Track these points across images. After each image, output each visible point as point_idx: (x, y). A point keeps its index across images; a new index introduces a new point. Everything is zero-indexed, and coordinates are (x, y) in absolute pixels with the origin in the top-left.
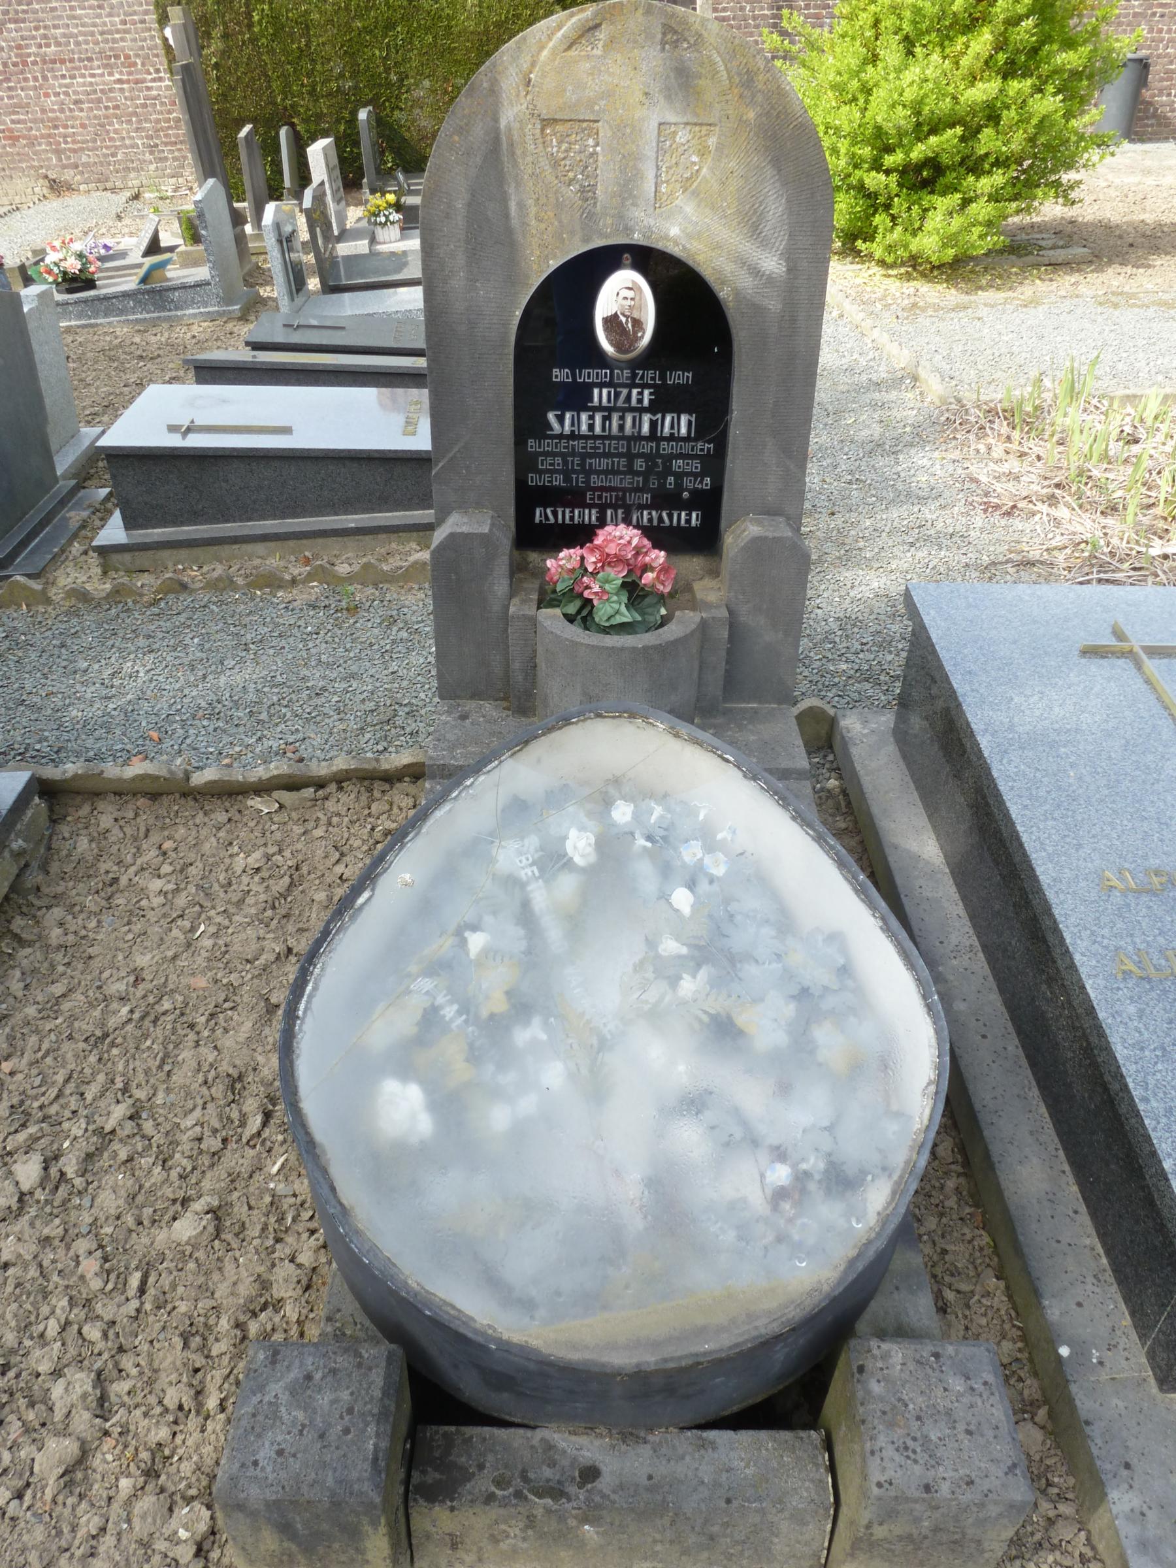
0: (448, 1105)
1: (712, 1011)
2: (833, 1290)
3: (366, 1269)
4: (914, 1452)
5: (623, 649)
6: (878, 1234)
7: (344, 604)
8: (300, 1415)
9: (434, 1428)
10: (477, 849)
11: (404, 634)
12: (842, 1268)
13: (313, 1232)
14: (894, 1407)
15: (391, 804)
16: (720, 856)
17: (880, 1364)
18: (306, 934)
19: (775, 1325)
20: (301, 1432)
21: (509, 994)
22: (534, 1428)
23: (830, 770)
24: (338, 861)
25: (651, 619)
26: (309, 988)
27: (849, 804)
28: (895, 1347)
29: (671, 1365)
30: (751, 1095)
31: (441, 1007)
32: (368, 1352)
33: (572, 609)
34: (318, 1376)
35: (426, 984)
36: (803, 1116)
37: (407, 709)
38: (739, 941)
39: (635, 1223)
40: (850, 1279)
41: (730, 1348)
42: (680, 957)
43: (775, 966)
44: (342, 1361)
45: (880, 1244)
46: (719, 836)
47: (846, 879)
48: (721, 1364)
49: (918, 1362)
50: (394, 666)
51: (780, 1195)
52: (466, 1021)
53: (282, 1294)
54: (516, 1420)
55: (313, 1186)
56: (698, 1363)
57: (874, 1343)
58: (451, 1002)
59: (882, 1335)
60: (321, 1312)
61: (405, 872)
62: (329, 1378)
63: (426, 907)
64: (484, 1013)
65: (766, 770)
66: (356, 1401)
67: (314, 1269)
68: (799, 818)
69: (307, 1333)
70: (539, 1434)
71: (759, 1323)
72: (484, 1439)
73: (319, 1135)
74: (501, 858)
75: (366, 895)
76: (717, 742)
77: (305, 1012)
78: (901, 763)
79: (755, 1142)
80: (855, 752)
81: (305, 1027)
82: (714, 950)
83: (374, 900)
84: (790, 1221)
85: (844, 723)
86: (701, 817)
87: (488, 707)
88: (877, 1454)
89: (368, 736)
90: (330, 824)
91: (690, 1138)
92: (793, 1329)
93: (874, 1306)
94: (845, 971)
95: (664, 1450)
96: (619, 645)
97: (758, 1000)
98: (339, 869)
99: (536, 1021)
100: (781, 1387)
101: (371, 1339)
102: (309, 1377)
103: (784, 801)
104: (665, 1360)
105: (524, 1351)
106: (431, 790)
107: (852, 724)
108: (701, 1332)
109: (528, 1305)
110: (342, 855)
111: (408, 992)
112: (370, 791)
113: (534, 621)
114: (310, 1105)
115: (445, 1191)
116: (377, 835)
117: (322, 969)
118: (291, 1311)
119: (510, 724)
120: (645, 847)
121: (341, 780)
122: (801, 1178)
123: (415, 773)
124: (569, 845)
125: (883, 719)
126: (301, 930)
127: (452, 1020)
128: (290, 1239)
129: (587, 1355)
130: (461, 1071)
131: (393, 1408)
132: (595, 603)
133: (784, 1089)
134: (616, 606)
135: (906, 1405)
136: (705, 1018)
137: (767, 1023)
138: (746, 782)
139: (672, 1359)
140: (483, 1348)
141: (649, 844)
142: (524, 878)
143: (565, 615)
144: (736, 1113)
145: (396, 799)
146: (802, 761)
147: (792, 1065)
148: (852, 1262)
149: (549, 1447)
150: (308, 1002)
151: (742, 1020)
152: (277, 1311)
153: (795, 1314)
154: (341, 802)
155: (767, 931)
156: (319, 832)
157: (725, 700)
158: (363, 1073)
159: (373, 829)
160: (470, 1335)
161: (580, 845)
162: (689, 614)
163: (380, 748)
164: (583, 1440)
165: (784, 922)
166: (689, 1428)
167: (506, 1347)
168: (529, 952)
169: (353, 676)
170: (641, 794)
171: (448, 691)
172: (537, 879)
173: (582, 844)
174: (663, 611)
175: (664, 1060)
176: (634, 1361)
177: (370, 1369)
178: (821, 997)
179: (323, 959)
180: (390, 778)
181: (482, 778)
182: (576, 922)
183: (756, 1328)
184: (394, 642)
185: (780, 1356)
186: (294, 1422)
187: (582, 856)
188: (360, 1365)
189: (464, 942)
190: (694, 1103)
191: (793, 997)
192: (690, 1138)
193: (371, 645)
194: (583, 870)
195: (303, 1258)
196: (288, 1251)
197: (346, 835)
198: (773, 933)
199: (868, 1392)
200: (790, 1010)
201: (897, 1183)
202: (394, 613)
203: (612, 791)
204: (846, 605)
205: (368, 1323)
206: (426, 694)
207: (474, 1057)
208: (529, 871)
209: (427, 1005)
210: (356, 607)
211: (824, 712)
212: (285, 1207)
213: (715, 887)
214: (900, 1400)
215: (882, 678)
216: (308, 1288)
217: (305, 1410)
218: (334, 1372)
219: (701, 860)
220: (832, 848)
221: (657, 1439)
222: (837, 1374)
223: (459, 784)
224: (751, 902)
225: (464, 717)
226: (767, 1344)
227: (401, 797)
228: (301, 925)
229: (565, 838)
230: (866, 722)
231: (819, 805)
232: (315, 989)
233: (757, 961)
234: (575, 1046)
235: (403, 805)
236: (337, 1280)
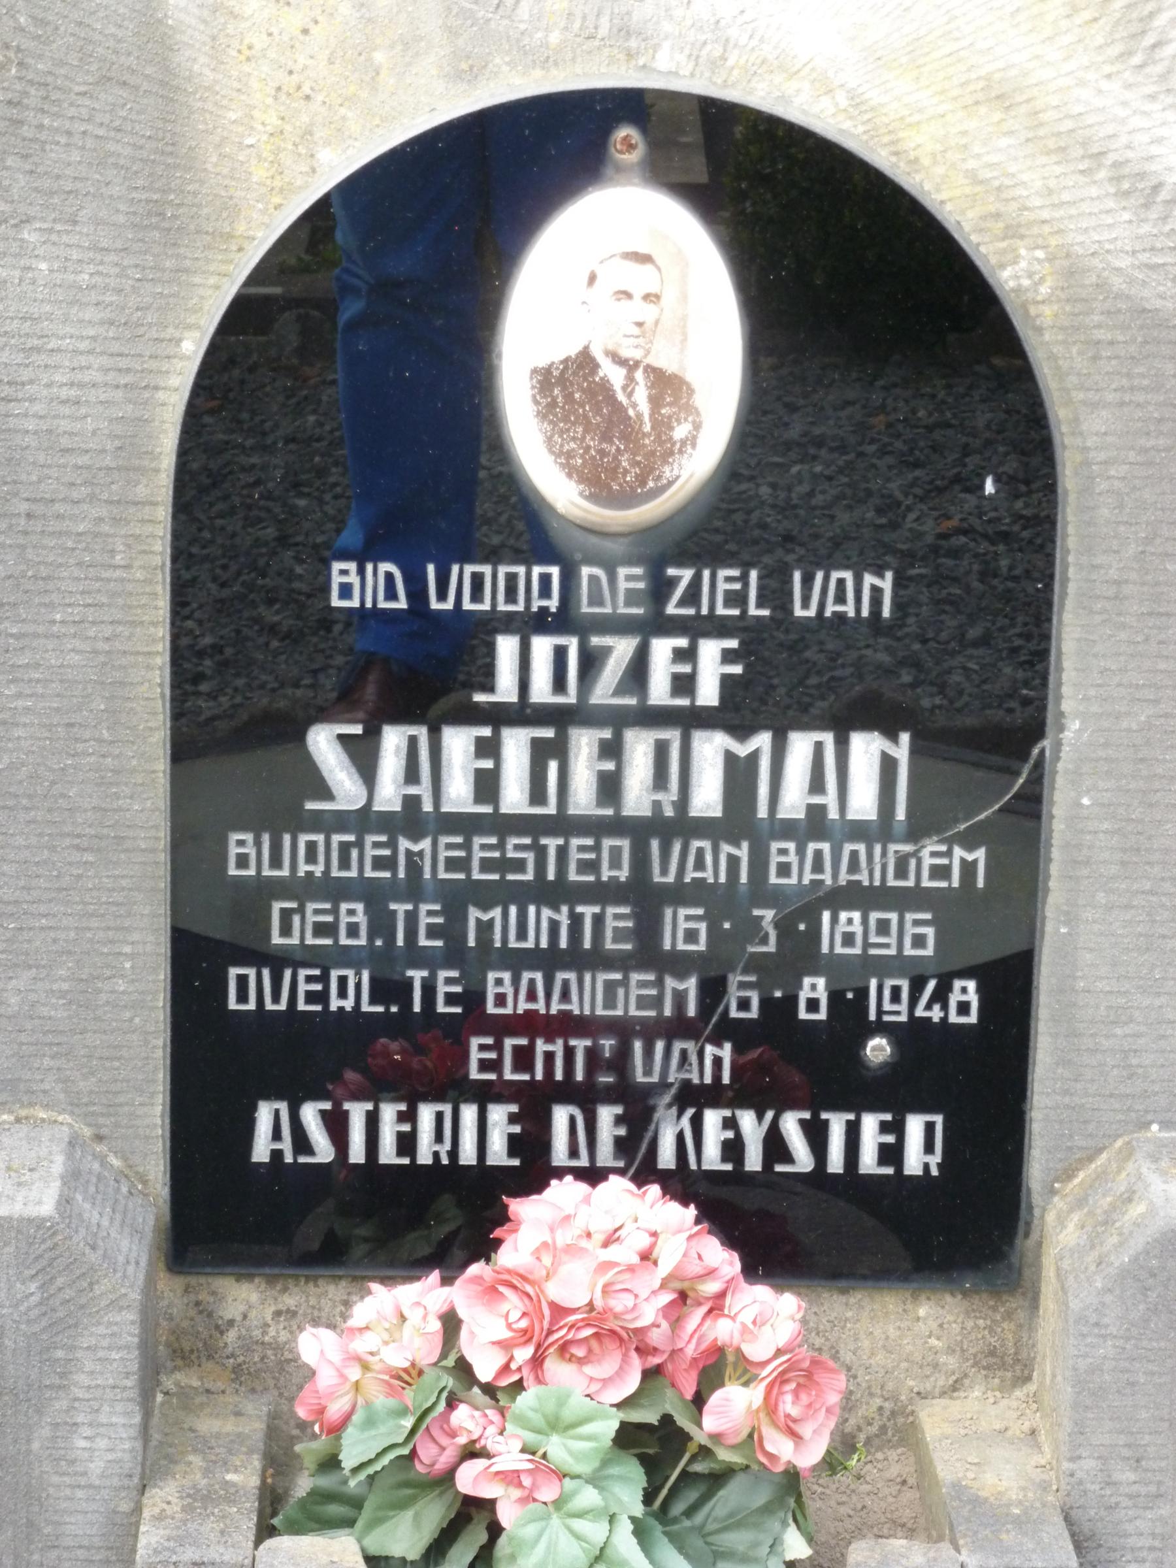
132: (506, 1514)
134: (596, 1531)
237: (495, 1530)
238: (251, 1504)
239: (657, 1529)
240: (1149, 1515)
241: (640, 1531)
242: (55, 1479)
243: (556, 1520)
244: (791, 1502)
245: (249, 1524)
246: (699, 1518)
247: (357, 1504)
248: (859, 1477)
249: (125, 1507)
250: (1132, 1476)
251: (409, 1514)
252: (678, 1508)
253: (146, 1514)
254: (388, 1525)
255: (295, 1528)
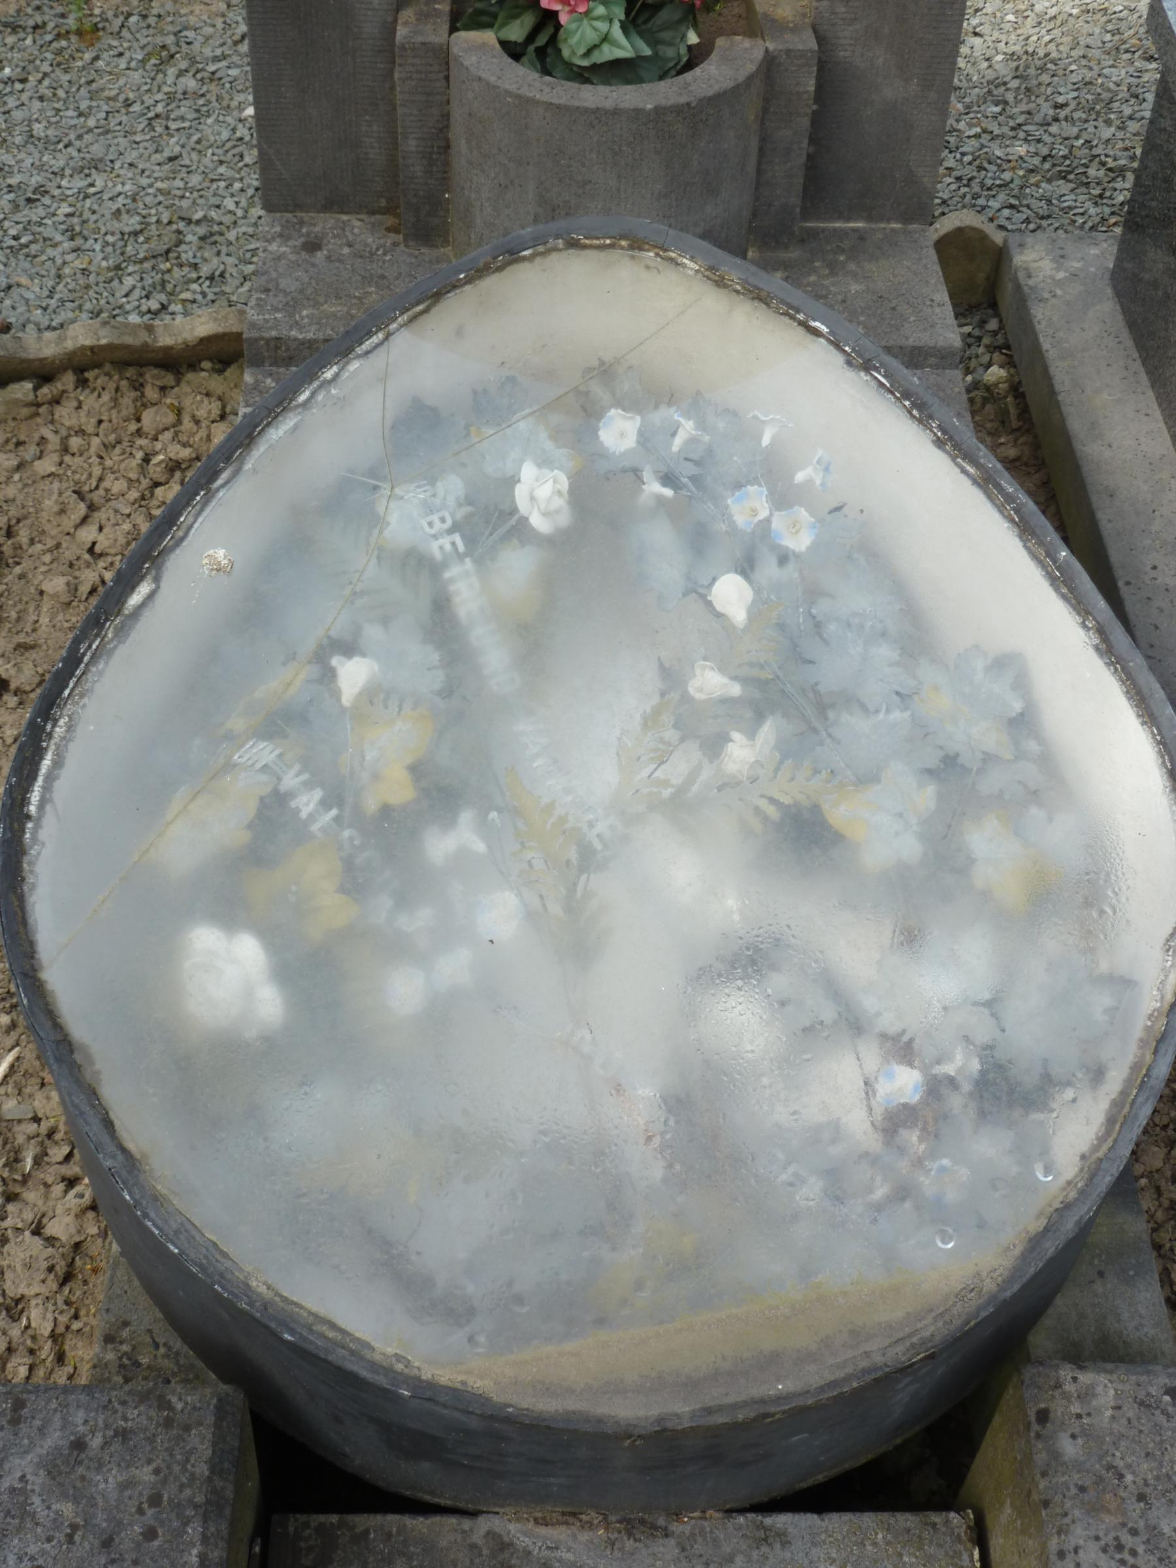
0: (312, 971)
1: (786, 800)
2: (1001, 1288)
3: (176, 1263)
4: (1134, 1553)
5: (616, 112)
6: (1082, 1192)
7: (71, 22)
8: (67, 1509)
9: (302, 1518)
10: (350, 499)
11: (190, 83)
12: (1018, 1251)
13: (71, 1182)
14: (1099, 1480)
15: (179, 412)
16: (803, 514)
17: (1076, 1408)
18: (33, 655)
19: (900, 1349)
20: (70, 1538)
21: (416, 770)
22: (474, 1514)
23: (991, 349)
24: (84, 520)
25: (670, 52)
26: (46, 763)
27: (1024, 411)
28: (1103, 1379)
29: (720, 1419)
30: (856, 949)
31: (291, 795)
32: (181, 1399)
33: (516, 31)
34: (96, 1442)
35: (263, 752)
36: (943, 985)
37: (201, 230)
38: (832, 671)
39: (646, 1167)
40: (1032, 1270)
41: (822, 1389)
42: (725, 701)
43: (896, 715)
44: (137, 1416)
45: (1084, 1210)
46: (800, 477)
47: (1034, 556)
48: (802, 1415)
49: (1142, 1404)
50: (172, 146)
51: (895, 1121)
52: (337, 819)
53: (23, 1290)
54: (442, 1502)
55: (73, 1115)
56: (766, 1415)
57: (1066, 1372)
58: (308, 786)
59: (1077, 1357)
60: (93, 1319)
61: (216, 545)
62: (116, 1446)
63: (253, 609)
64: (371, 805)
65: (888, 350)
66: (164, 1482)
67: (77, 1246)
68: (946, 441)
69: (70, 1354)
70: (484, 1524)
71: (873, 1346)
72: (389, 1535)
73: (78, 1028)
74: (394, 518)
75: (144, 589)
76: (796, 295)
77: (41, 806)
78: (1125, 335)
79: (854, 1024)
80: (1041, 314)
81: (43, 835)
82: (790, 687)
83: (159, 599)
84: (919, 1163)
85: (1020, 259)
86: (766, 441)
87: (357, 226)
88: (1070, 1556)
89: (129, 281)
90: (65, 450)
91: (741, 1021)
92: (931, 1357)
93: (1059, 1301)
94: (1023, 724)
95: (698, 1548)
96: (609, 104)
97: (868, 779)
98: (88, 534)
99: (466, 817)
100: (898, 1441)
101: (191, 1380)
102: (79, 1445)
103: (920, 410)
104: (709, 1411)
105: (459, 1397)
106: (256, 387)
107: (1037, 262)
108: (771, 1361)
109: (454, 1311)
110: (92, 508)
111: (229, 767)
112: (138, 386)
113: (443, 57)
114: (58, 976)
115: (311, 1120)
116: (156, 470)
117: (70, 728)
118: (40, 1319)
119: (401, 261)
120: (660, 499)
121: (83, 365)
122: (936, 1088)
123: (224, 353)
124: (521, 494)
125: (1094, 251)
126: (23, 648)
127: (311, 817)
128: (31, 1195)
129: (572, 1404)
130: (332, 909)
131: (229, 1493)
132: (563, 18)
133: (910, 937)
134: (603, 26)
135: (1121, 1477)
136: (772, 811)
137: (884, 825)
138: (850, 374)
139: (720, 1409)
140: (389, 1396)
141: (668, 492)
142: (438, 556)
143: (505, 45)
144: (832, 987)
145: (187, 402)
146: (946, 330)
147: (924, 896)
148: (1035, 1242)
149: (501, 1545)
150: (47, 788)
151: (841, 813)
152: (15, 1319)
153: (933, 1330)
154: (87, 408)
155: (885, 652)
156: (47, 465)
157: (806, 215)
158: (156, 913)
159: (146, 460)
160: (364, 1373)
161: (541, 492)
162: (743, 43)
163: (154, 305)
164: (559, 1533)
165: (915, 637)
166: (742, 1511)
167: (428, 1391)
168: (447, 692)
169: (96, 165)
170: (652, 395)
171: (282, 194)
172: (461, 557)
173: (545, 491)
174: (693, 38)
175: (695, 884)
176: (654, 1412)
177: (187, 1428)
178: (980, 771)
179: (69, 708)
180: (176, 363)
181: (354, 366)
182: (533, 637)
183: (867, 1354)
184: (171, 97)
185: (902, 1397)
186: (57, 1521)
187: (546, 514)
188: (168, 1423)
189: (329, 675)
190: (749, 960)
191: (929, 772)
192: (741, 1021)
193: (128, 104)
194: (549, 541)
195: (53, 1228)
196: (29, 1216)
197: (97, 471)
198: (895, 656)
199: (1056, 1455)
200: (926, 797)
201: (1117, 1104)
202: (170, 40)
203: (599, 391)
204: (1027, 28)
205: (178, 1344)
206: (236, 198)
207: (355, 882)
208: (446, 542)
209: (265, 791)
210: (96, 28)
211: (983, 237)
212: (20, 1139)
213: (791, 572)
214: (1110, 1467)
215: (1092, 172)
216: (67, 1278)
217: (76, 1501)
218: (123, 1435)
219: (768, 520)
220: (1009, 499)
221: (687, 1529)
222: (997, 1421)
223: (311, 376)
224: (855, 599)
225: (312, 246)
226: (885, 1381)
227: (195, 396)
228: (21, 638)
229: (514, 480)
230: (1061, 258)
231: (973, 413)
232: (58, 763)
233: (864, 708)
234: (538, 864)
235: (201, 413)
236: (121, 1273)
237: (558, 26)
238: (447, 18)
239: (631, 29)
240: (851, 28)
241: (624, 27)
242: (358, 5)
243: (585, 22)
244: (691, 17)
245: (446, 27)
246: (649, 25)
247: (495, 16)
248: (720, 14)
249: (390, 19)
250: (844, 10)
251: (518, 22)
252: (640, 20)
253: (400, 22)
254: (509, 27)
255: (467, 28)
